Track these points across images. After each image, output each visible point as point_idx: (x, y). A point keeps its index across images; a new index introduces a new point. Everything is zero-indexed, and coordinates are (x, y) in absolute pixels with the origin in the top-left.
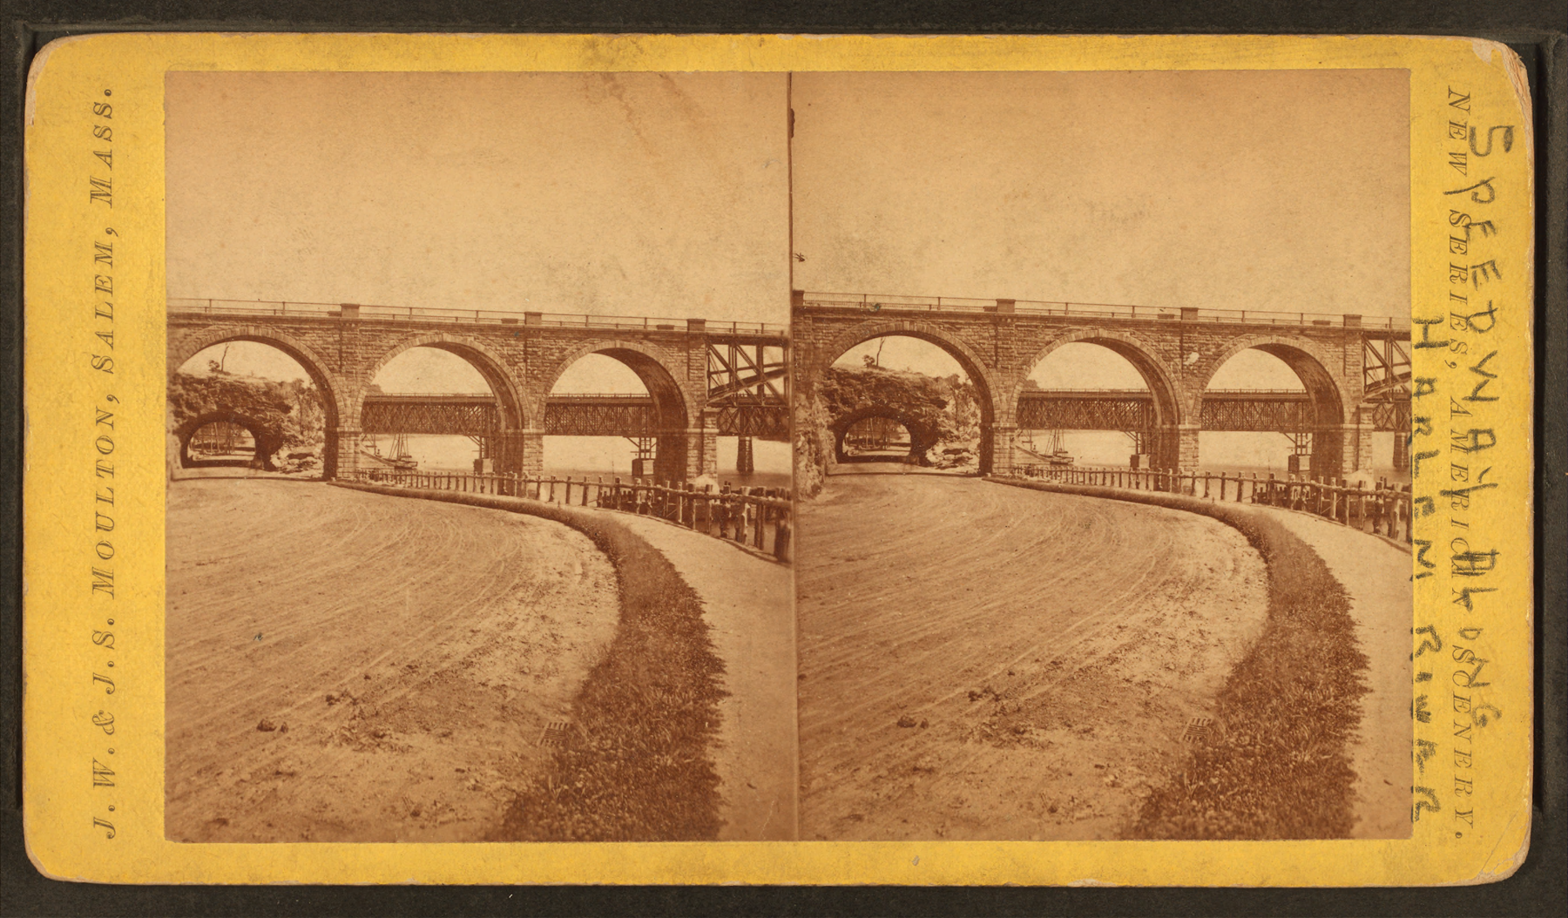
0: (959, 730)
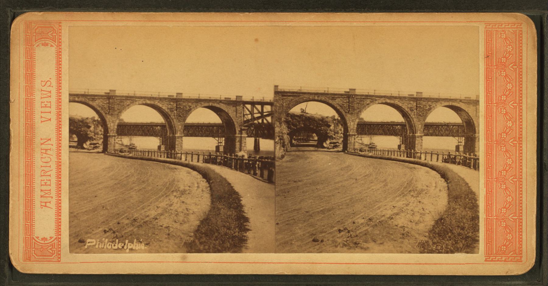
0: (335, 243)
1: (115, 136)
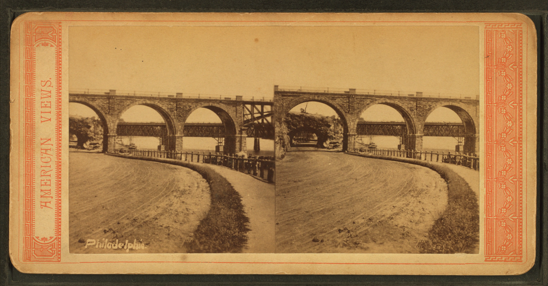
1: (115, 136)
